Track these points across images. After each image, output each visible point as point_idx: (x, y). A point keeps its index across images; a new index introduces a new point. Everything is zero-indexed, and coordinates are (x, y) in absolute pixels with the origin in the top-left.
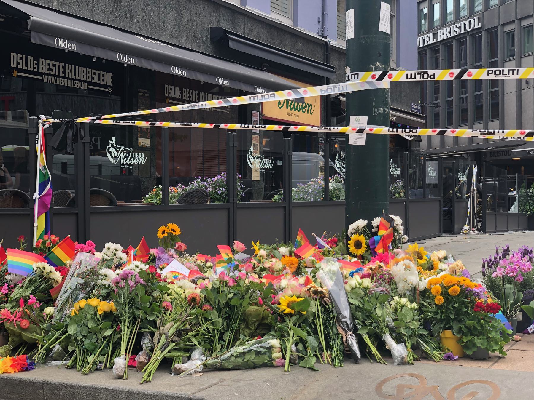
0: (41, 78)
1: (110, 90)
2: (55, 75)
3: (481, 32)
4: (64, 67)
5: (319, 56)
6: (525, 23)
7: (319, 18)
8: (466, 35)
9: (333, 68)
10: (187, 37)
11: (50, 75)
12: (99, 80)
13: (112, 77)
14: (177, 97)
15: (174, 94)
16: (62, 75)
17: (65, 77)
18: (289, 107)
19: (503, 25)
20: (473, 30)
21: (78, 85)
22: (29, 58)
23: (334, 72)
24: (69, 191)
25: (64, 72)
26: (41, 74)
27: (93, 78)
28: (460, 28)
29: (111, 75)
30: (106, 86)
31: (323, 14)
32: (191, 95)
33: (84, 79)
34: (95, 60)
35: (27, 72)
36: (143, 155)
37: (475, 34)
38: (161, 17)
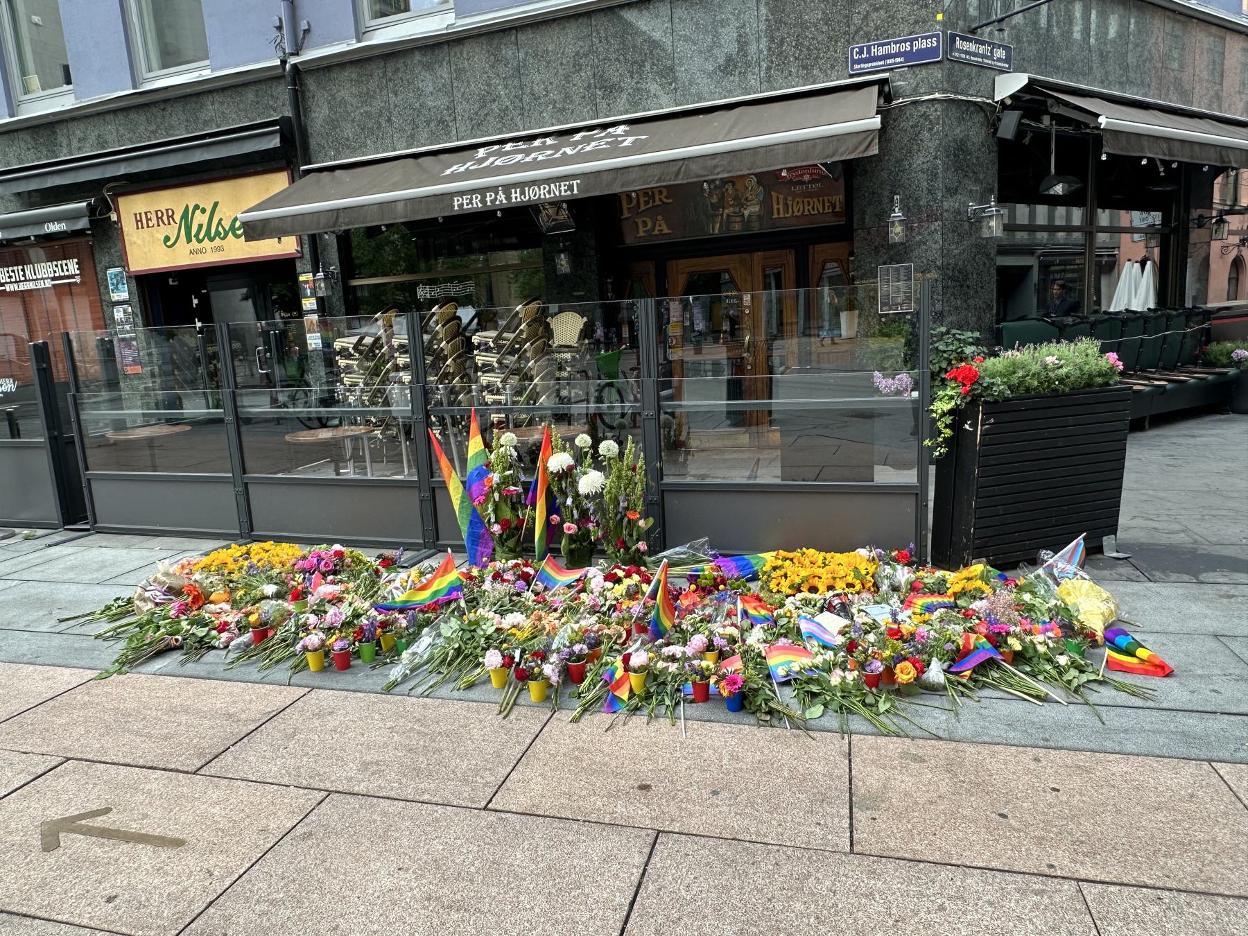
1: (78, 279)
2: (16, 282)
4: (23, 270)
11: (11, 282)
16: (23, 279)
17: (26, 280)
18: (194, 239)
21: (41, 285)
25: (24, 275)
27: (55, 272)
29: (76, 260)
30: (72, 276)
33: (46, 276)
34: (499, 214)
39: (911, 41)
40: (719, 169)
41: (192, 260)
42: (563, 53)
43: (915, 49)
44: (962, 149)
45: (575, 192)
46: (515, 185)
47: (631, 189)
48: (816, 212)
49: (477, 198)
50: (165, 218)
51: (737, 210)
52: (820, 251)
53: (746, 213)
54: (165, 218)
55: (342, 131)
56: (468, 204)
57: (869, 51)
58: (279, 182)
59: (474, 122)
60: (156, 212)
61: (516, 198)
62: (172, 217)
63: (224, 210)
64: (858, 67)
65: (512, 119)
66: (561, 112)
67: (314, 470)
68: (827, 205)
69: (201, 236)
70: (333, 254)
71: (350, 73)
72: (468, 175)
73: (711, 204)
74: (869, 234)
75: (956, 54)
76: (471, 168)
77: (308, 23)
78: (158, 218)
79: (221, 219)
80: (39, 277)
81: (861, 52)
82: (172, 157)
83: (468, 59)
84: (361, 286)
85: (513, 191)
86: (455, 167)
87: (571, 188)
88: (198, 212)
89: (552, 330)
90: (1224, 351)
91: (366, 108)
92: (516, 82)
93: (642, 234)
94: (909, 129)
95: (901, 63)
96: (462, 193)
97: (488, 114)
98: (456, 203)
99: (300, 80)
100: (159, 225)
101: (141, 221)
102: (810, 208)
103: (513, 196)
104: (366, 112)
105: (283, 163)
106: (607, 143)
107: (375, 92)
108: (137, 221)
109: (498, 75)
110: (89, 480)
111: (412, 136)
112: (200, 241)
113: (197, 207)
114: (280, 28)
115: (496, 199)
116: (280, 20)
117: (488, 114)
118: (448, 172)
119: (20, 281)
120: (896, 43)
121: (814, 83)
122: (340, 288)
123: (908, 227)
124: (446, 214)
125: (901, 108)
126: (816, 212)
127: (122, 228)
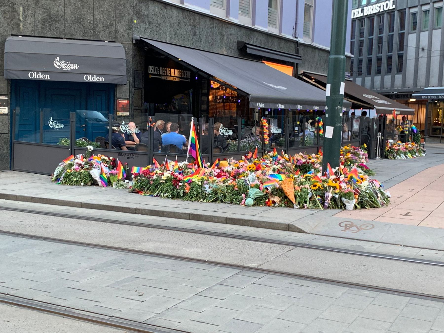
0: (160, 77)
3: (394, 12)
5: (292, 49)
6: (424, 8)
7: (293, 26)
8: (384, 12)
9: (301, 57)
11: (164, 75)
12: (185, 76)
14: (156, 73)
15: (155, 72)
17: (170, 76)
19: (410, 8)
20: (388, 10)
22: (156, 67)
23: (301, 59)
25: (170, 73)
26: (160, 75)
27: (182, 75)
28: (380, 7)
29: (190, 72)
31: (296, 24)
32: (165, 71)
35: (155, 75)
36: (62, 124)
37: (390, 12)
38: (214, 38)
71: (208, 20)
80: (176, 76)
90: (201, 123)
110: (75, 149)
119: (168, 76)
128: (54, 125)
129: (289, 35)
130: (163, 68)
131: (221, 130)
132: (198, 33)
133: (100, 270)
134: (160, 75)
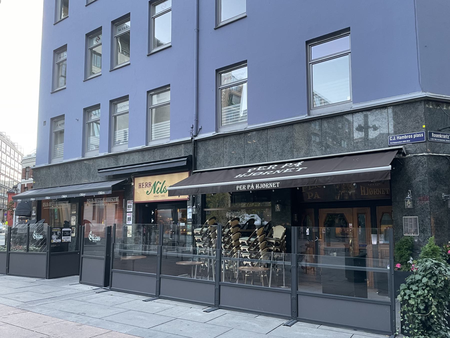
10: (93, 177)
13: (118, 198)
18: (156, 192)
24: (74, 234)
26: (49, 207)
27: (111, 200)
29: (118, 197)
39: (413, 134)
40: (329, 182)
41: (154, 199)
42: (283, 137)
43: (414, 137)
44: (438, 173)
45: (278, 186)
46: (257, 183)
47: (297, 186)
48: (378, 194)
49: (244, 186)
50: (148, 185)
51: (346, 191)
52: (379, 209)
53: (350, 193)
54: (148, 185)
55: (207, 160)
56: (241, 188)
57: (396, 138)
58: (185, 175)
59: (251, 158)
60: (146, 183)
61: (257, 187)
62: (150, 185)
63: (167, 183)
64: (392, 143)
65: (264, 158)
66: (281, 156)
67: (185, 276)
68: (383, 191)
69: (158, 192)
70: (200, 200)
71: (213, 142)
72: (243, 179)
73: (336, 189)
74: (399, 204)
75: (433, 139)
76: (244, 176)
77: (201, 126)
78: (146, 185)
79: (165, 186)
81: (393, 138)
82: (153, 167)
83: (251, 138)
84: (208, 211)
85: (257, 185)
86: (239, 175)
87: (276, 185)
88: (159, 184)
89: (273, 231)
91: (216, 153)
92: (266, 146)
93: (309, 198)
94: (413, 166)
95: (409, 142)
96: (239, 185)
97: (256, 156)
98: (237, 188)
99: (196, 143)
100: (146, 187)
101: (141, 186)
102: (376, 192)
103: (257, 186)
104: (216, 154)
105: (188, 169)
106: (292, 170)
107: (219, 148)
108: (139, 186)
109: (260, 144)
110: (112, 272)
111: (230, 162)
112: (158, 193)
113: (158, 182)
114: (192, 128)
115: (251, 187)
116: (193, 125)
117: (256, 156)
118: (237, 177)
120: (406, 135)
121: (375, 149)
122: (200, 211)
123: (413, 202)
124: (234, 191)
125: (410, 158)
126: (378, 194)
127: (134, 188)
128: (37, 236)
129: (303, 114)
130: (97, 199)
131: (34, 235)
132: (69, 175)
133: (97, 326)
134: (49, 207)
